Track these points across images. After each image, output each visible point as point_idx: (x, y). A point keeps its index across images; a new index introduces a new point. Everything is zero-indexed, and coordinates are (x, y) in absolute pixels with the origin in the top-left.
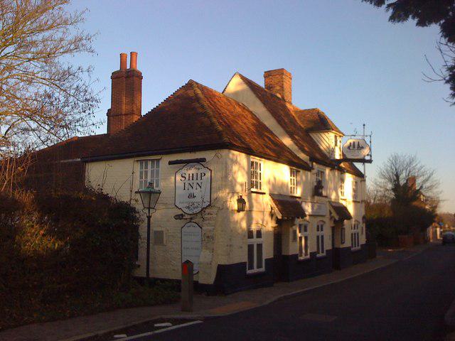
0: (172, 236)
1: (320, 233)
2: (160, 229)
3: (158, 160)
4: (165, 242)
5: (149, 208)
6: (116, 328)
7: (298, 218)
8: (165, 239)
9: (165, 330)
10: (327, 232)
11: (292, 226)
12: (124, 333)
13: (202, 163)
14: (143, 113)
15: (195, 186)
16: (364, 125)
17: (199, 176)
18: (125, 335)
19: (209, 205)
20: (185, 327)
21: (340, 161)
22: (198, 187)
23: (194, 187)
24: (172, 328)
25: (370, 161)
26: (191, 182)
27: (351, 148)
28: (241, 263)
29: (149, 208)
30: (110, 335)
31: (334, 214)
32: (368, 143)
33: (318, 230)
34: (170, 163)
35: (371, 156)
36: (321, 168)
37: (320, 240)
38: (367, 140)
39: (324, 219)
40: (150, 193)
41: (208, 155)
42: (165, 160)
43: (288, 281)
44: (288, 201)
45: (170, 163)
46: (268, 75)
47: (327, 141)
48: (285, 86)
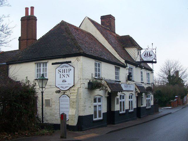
1: (131, 100)
5: (42, 88)
10: (134, 100)
14: (39, 36)
15: (66, 76)
16: (152, 44)
23: (66, 77)
25: (155, 62)
26: (64, 74)
27: (146, 55)
29: (42, 88)
31: (138, 90)
34: (53, 64)
36: (131, 66)
37: (131, 103)
43: (114, 124)
46: (103, 18)
47: (132, 52)
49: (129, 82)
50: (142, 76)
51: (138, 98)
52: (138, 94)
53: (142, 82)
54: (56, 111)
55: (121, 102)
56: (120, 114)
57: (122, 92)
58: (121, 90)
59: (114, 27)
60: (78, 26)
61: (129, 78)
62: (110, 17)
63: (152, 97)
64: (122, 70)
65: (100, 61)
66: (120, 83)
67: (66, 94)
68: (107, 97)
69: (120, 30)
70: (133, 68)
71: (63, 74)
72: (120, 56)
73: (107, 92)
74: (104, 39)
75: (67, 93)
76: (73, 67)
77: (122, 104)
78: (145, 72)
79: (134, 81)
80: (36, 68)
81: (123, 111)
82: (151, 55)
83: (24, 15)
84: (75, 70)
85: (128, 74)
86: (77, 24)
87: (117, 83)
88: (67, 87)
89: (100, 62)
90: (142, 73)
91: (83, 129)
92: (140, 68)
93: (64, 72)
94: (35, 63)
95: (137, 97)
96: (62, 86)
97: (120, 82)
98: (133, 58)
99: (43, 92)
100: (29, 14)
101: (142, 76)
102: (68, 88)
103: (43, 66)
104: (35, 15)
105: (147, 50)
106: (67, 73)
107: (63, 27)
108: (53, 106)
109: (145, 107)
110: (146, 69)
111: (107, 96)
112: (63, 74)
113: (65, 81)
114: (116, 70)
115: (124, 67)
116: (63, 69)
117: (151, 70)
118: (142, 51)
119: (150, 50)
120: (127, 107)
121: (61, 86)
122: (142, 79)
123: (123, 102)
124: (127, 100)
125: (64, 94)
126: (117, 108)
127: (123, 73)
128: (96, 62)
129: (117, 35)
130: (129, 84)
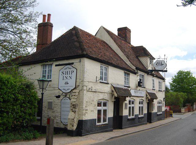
1: (141, 105)
2: (50, 101)
3: (51, 65)
5: (43, 89)
6: (127, 136)
10: (145, 106)
11: (124, 101)
14: (53, 40)
15: (68, 78)
16: (165, 55)
21: (152, 71)
23: (68, 79)
25: (166, 71)
26: (66, 76)
27: (158, 64)
28: (93, 120)
29: (43, 89)
31: (148, 96)
34: (56, 65)
36: (142, 73)
37: (141, 109)
39: (143, 99)
40: (43, 81)
43: (122, 129)
44: (122, 89)
46: (119, 30)
47: (145, 61)
48: (127, 35)
49: (139, 88)
50: (153, 84)
51: (149, 104)
52: (149, 100)
53: (154, 89)
54: (57, 114)
55: (130, 108)
56: (128, 119)
57: (130, 97)
58: (130, 95)
59: (130, 39)
60: (94, 34)
61: (140, 84)
62: (126, 29)
63: (163, 103)
64: (132, 76)
65: (106, 65)
66: (130, 89)
67: (67, 96)
68: (114, 101)
69: (135, 42)
70: (144, 75)
71: (66, 76)
72: (131, 63)
73: (113, 97)
74: (117, 46)
75: (68, 96)
76: (76, 69)
77: (131, 110)
78: (157, 81)
79: (145, 88)
80: (42, 70)
81: (133, 115)
82: (163, 64)
83: (42, 22)
84: (77, 72)
85: (139, 81)
86: (93, 32)
87: (127, 88)
88: (69, 89)
89: (107, 66)
90: (153, 80)
91: (83, 135)
92: (152, 76)
93: (67, 74)
94: (42, 65)
95: (148, 104)
96: (65, 88)
97: (129, 87)
98: (145, 66)
99: (43, 94)
100: (46, 21)
101: (153, 84)
102: (70, 90)
103: (49, 68)
104: (51, 21)
105: (159, 59)
106: (69, 75)
107: (74, 32)
108: (55, 109)
109: (157, 113)
110: (158, 78)
111: (114, 100)
112: (66, 76)
113: (68, 83)
114: (125, 75)
115: (135, 73)
116: (67, 70)
117: (163, 79)
118: (154, 61)
119: (162, 60)
120: (136, 112)
121: (63, 88)
122: (154, 87)
123: (133, 108)
124: (137, 106)
125: (65, 97)
126: (125, 112)
127: (134, 79)
128: (102, 66)
129: (132, 46)
130: (139, 90)
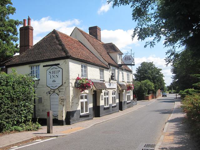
0: (46, 100)
3: (39, 66)
4: (43, 103)
7: (104, 90)
8: (43, 101)
9: (36, 143)
12: (16, 146)
13: (58, 66)
14: (34, 44)
17: (57, 72)
18: (41, 140)
19: (62, 85)
20: (47, 141)
22: (57, 77)
23: (55, 77)
24: (17, 148)
25: (134, 65)
27: (126, 59)
30: (9, 147)
32: (133, 57)
33: (113, 94)
34: (44, 66)
35: (134, 63)
38: (133, 56)
41: (61, 62)
42: (42, 64)
45: (44, 66)
46: (90, 29)
48: (98, 33)
